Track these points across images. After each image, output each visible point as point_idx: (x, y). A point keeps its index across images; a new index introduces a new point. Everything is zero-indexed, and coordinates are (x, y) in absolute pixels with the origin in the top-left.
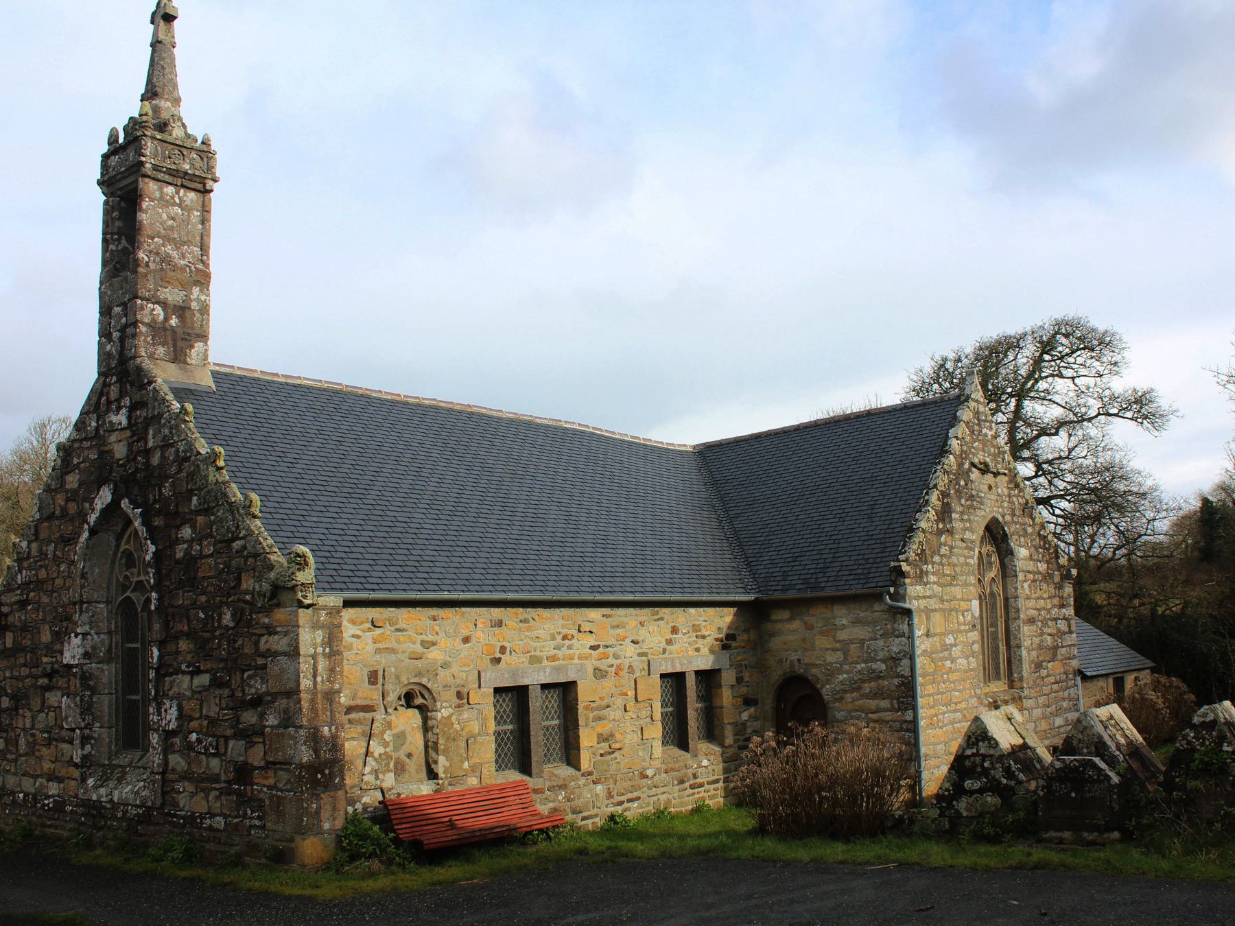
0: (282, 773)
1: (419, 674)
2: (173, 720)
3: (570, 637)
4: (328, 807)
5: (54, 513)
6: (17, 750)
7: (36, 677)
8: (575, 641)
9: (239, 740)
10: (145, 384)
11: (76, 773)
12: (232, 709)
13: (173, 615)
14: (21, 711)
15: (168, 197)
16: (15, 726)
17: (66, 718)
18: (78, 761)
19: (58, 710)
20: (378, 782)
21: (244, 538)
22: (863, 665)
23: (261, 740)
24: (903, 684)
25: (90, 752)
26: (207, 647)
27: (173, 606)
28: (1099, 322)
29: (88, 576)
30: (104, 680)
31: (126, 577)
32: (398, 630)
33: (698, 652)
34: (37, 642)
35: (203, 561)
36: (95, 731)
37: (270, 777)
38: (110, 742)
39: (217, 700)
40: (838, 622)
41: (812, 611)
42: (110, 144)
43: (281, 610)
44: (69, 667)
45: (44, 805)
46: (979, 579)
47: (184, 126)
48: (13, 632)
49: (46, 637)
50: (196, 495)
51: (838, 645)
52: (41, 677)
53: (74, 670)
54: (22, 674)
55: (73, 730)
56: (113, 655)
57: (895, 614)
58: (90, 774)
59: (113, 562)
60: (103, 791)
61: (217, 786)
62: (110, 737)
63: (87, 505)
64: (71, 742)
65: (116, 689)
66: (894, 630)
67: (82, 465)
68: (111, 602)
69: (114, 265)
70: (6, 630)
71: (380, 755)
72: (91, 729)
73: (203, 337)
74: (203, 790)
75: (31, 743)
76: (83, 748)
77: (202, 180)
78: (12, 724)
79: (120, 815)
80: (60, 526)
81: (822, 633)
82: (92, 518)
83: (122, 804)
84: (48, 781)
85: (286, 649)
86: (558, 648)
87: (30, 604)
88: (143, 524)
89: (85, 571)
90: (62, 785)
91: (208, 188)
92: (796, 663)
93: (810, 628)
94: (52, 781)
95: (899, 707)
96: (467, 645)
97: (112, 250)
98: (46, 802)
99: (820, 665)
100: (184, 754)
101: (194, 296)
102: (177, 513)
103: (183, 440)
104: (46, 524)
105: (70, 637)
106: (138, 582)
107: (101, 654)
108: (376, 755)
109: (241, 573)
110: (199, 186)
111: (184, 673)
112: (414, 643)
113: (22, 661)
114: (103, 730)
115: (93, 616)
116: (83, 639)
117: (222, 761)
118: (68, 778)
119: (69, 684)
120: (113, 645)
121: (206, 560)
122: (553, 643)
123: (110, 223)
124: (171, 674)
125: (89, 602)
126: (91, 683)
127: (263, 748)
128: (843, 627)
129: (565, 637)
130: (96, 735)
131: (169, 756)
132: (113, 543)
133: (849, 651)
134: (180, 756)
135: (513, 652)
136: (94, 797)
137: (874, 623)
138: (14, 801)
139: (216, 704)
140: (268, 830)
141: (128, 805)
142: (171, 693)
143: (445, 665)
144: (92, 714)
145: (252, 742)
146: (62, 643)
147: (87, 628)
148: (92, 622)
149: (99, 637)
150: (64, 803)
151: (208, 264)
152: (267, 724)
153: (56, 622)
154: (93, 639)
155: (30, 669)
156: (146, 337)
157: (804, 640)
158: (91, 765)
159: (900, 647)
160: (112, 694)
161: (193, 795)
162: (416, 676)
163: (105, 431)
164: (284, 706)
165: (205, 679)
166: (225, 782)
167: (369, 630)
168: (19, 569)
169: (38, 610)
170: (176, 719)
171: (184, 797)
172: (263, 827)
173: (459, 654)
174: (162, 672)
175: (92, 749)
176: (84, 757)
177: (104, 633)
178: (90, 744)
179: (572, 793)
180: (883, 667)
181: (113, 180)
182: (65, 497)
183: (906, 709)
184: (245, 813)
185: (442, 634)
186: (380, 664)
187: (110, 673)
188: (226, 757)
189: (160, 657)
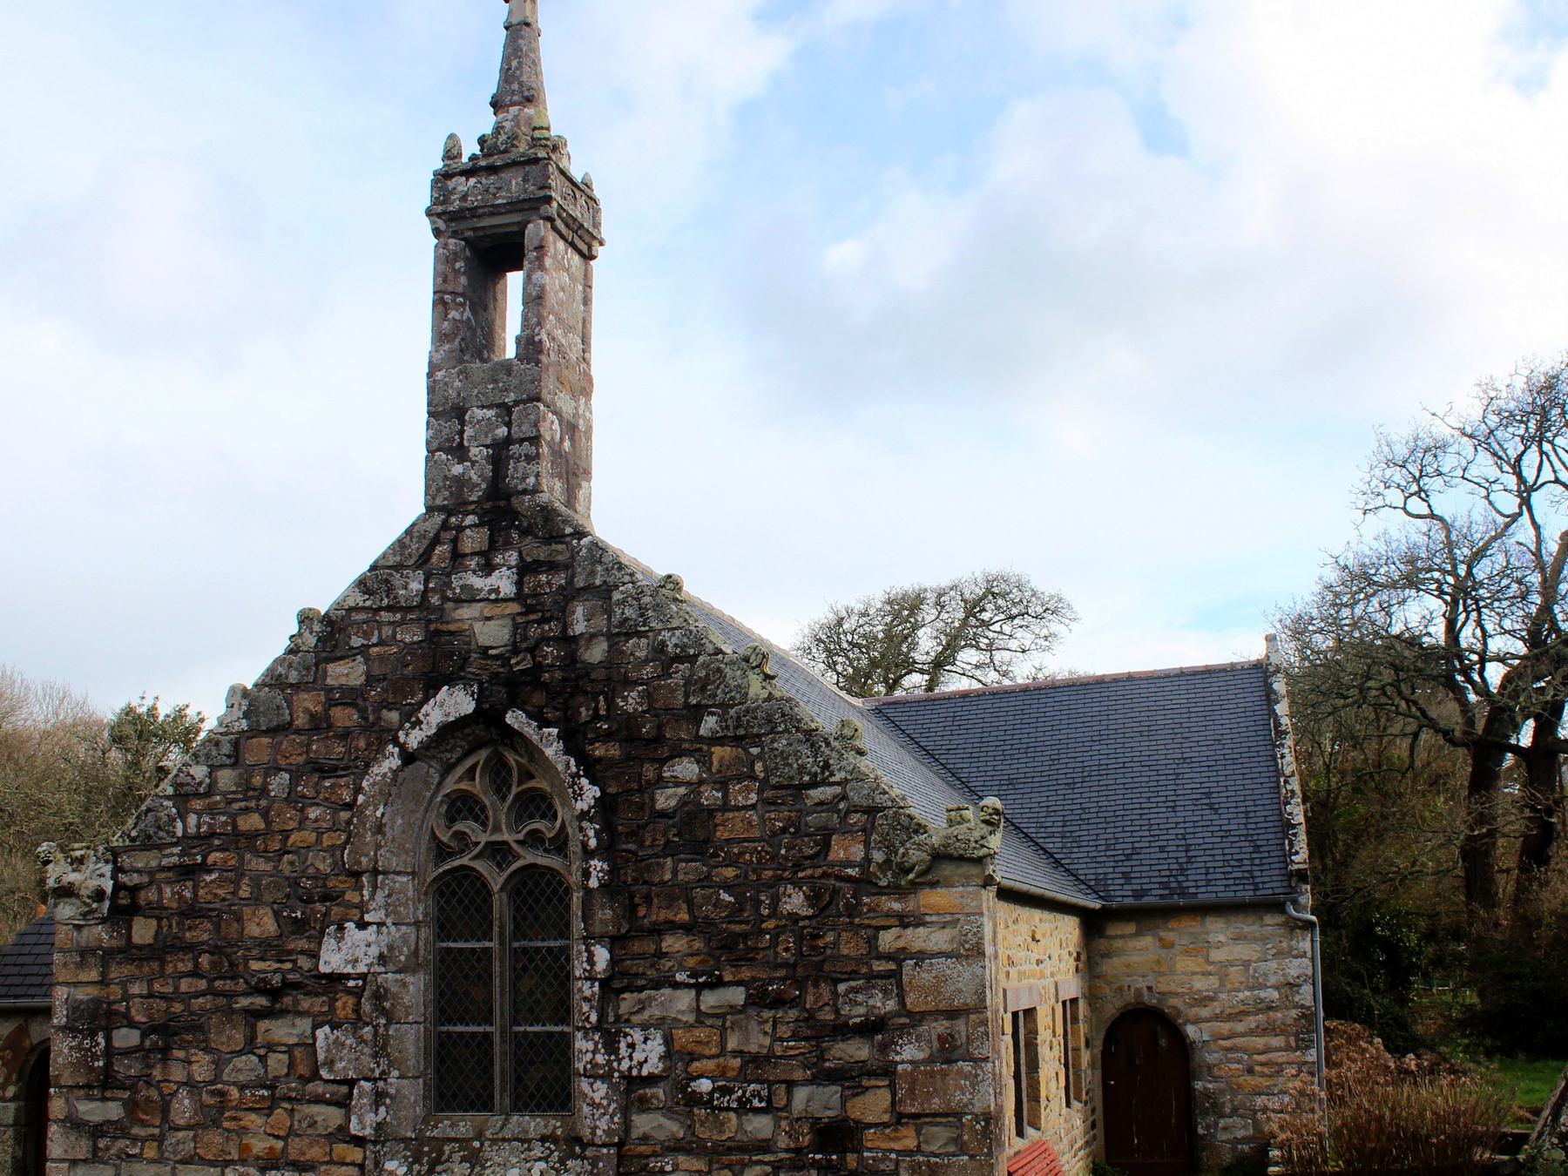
5: (291, 723)
7: (231, 995)
12: (806, 1039)
17: (330, 1063)
21: (843, 783)
22: (1247, 993)
23: (886, 1083)
24: (1304, 1016)
26: (741, 946)
27: (646, 882)
28: (1043, 582)
29: (387, 829)
36: (391, 1084)
39: (768, 1028)
40: (1212, 938)
41: (1172, 924)
43: (939, 890)
44: (336, 978)
51: (1210, 968)
52: (246, 994)
55: (351, 1083)
56: (421, 960)
57: (1292, 929)
66: (1291, 948)
67: (376, 649)
72: (385, 1080)
81: (1187, 952)
82: (414, 739)
87: (210, 872)
88: (568, 751)
92: (1145, 991)
93: (1166, 945)
95: (1297, 1045)
99: (1183, 994)
100: (676, 1112)
104: (265, 740)
105: (341, 928)
107: (402, 958)
109: (831, 835)
114: (405, 1082)
115: (389, 896)
125: (385, 873)
126: (387, 1005)
127: (889, 1097)
128: (1220, 945)
130: (392, 1091)
131: (634, 1117)
132: (437, 778)
133: (1227, 975)
137: (1264, 939)
145: (860, 1086)
147: (382, 914)
148: (388, 904)
149: (398, 930)
152: (898, 1058)
154: (389, 933)
157: (1158, 962)
158: (386, 1140)
159: (1300, 971)
169: (236, 883)
170: (661, 1058)
174: (616, 984)
177: (407, 924)
180: (1276, 995)
183: (1308, 1047)
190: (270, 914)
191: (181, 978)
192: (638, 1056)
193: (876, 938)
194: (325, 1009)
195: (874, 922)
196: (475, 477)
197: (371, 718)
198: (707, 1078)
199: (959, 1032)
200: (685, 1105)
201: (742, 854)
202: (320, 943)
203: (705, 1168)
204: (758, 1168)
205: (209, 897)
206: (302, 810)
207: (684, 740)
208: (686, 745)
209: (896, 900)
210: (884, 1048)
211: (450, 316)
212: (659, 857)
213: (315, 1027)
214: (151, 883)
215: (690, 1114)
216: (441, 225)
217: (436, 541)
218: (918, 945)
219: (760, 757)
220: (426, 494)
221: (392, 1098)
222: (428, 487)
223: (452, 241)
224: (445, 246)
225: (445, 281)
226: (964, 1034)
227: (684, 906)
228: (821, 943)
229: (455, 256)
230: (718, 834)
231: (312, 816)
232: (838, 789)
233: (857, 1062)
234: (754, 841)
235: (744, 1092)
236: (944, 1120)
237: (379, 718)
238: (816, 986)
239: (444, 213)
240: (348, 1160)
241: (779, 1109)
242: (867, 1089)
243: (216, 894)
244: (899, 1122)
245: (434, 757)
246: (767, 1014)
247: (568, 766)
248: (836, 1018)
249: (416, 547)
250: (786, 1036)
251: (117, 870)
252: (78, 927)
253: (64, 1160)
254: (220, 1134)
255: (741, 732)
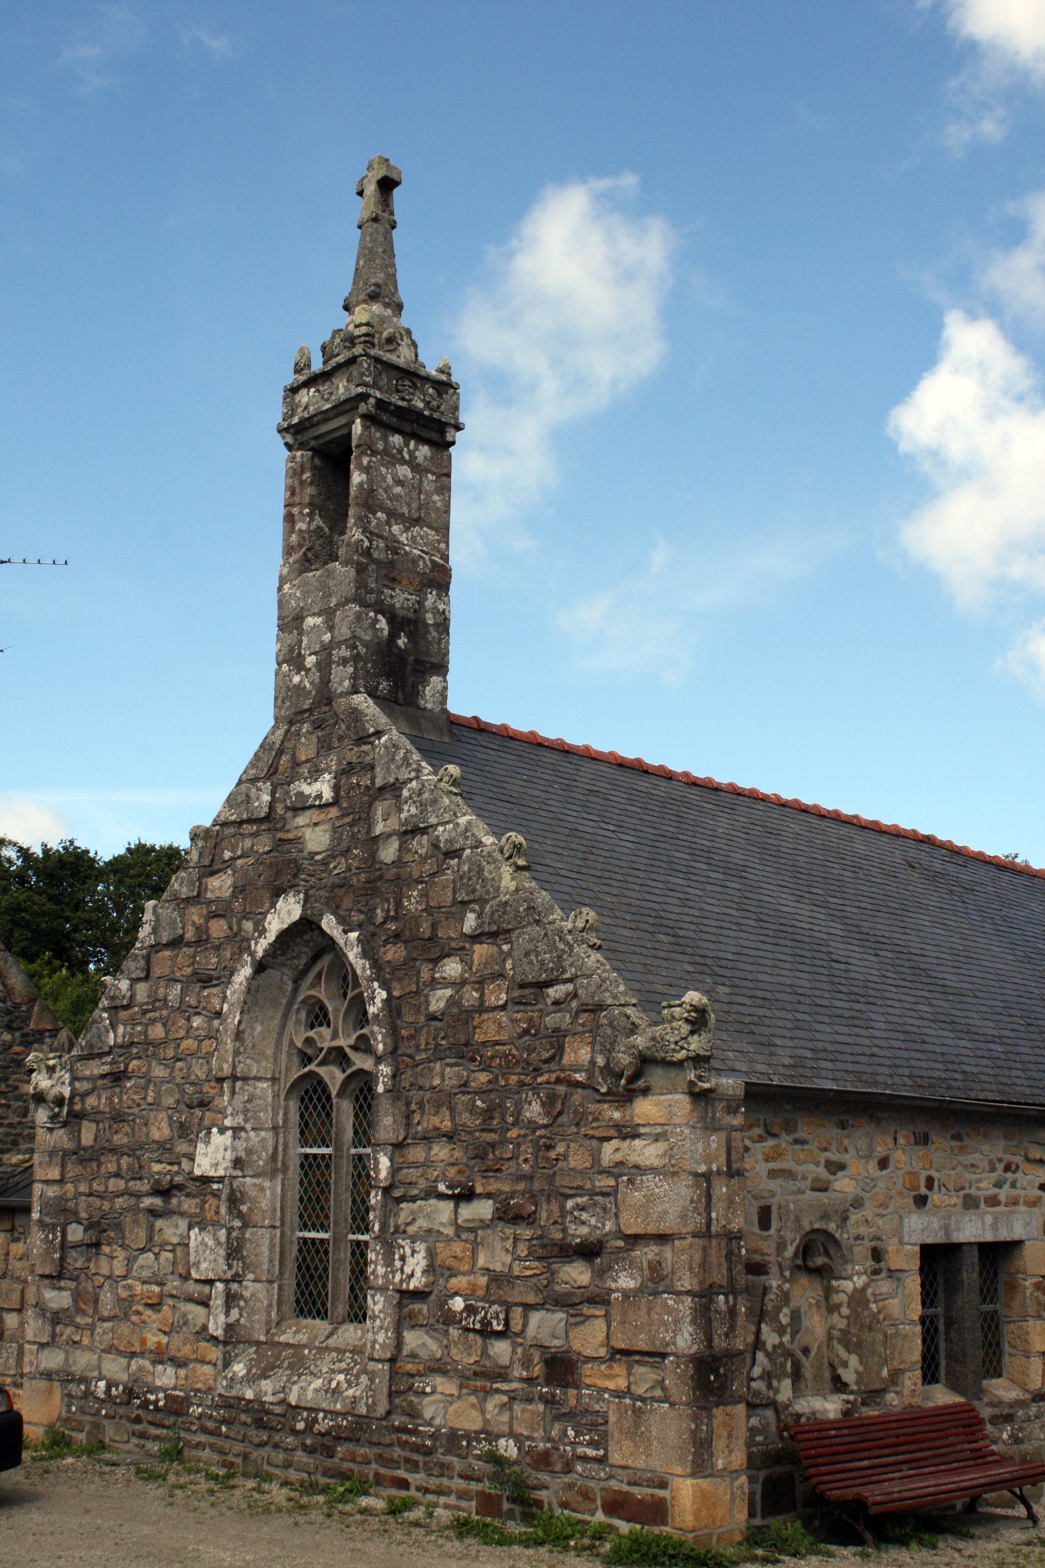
0: (643, 1369)
1: (825, 1217)
2: (418, 1274)
3: (1013, 1167)
4: (723, 1432)
5: (182, 937)
6: (96, 1310)
7: (138, 1196)
8: (1019, 1174)
9: (554, 1311)
10: (370, 736)
11: (215, 1353)
12: (539, 1259)
13: (421, 1105)
14: (106, 1249)
15: (395, 451)
16: (93, 1271)
17: (197, 1264)
18: (219, 1333)
19: (179, 1249)
20: (771, 1393)
23: (603, 1313)
25: (238, 1321)
26: (491, 1156)
27: (421, 1088)
29: (246, 1036)
30: (264, 1204)
31: (309, 1041)
32: (797, 1141)
33: (966, 1197)
34: (143, 1139)
35: (485, 1016)
37: (618, 1375)
38: (270, 1305)
39: (509, 1244)
42: (298, 370)
44: (206, 1180)
45: (147, 1402)
46: (369, 1110)
47: (414, 345)
48: (97, 1122)
49: (160, 1130)
50: (473, 911)
52: (148, 1194)
53: (215, 1186)
54: (111, 1189)
55: (210, 1282)
58: (236, 1356)
59: (285, 1017)
60: (267, 1385)
61: (505, 1387)
62: (270, 1296)
63: (248, 926)
64: (205, 1303)
65: (282, 1220)
67: (239, 862)
68: (279, 1079)
69: (305, 554)
70: (81, 1119)
71: (774, 1347)
72: (240, 1282)
73: (441, 668)
74: (475, 1391)
75: (124, 1300)
76: (227, 1314)
77: (441, 427)
78: (88, 1268)
79: (300, 1426)
80: (194, 957)
82: (261, 947)
83: (306, 1409)
84: (154, 1363)
85: (656, 1162)
86: (999, 1185)
87: (130, 1078)
88: (364, 954)
89: (241, 1028)
90: (182, 1372)
91: (449, 438)
94: (161, 1362)
96: (885, 1172)
97: (300, 531)
98: (152, 1397)
101: (429, 603)
102: (433, 938)
103: (448, 823)
104: (167, 953)
105: (209, 1133)
106: (331, 1050)
107: (261, 1163)
108: (769, 1348)
110: (435, 436)
111: (441, 1196)
112: (817, 1164)
113: (112, 1167)
115: (249, 1101)
116: (235, 1137)
117: (515, 1345)
118: (196, 1360)
119: (202, 1208)
120: (280, 1148)
121: (491, 1015)
122: (994, 1176)
123: (297, 490)
124: (413, 1199)
125: (245, 1079)
126: (244, 1208)
127: (605, 1329)
129: (1007, 1168)
130: (247, 1294)
131: (405, 1334)
132: (290, 986)
134: (427, 1333)
135: (943, 1188)
136: (249, 1394)
138: (88, 1394)
139: (507, 1251)
140: (612, 1466)
141: (317, 1410)
142: (411, 1229)
143: (857, 1203)
144: (243, 1258)
146: (193, 1143)
147: (240, 1119)
150: (186, 1402)
151: (448, 556)
152: (613, 1285)
153: (183, 1107)
154: (247, 1139)
155: (127, 1182)
156: (366, 663)
160: (274, 1227)
161: (450, 1399)
162: (822, 1218)
163: (287, 809)
164: (651, 1256)
165: (484, 1209)
166: (522, 1380)
167: (761, 1139)
168: (111, 1023)
169: (145, 1088)
170: (424, 1272)
171: (433, 1402)
172: (601, 1461)
173: (875, 1186)
174: (397, 1193)
175: (241, 1315)
176: (229, 1328)
177: (266, 1130)
178: (238, 1306)
179: (1020, 1429)
181: (307, 424)
182: (205, 912)
184: (564, 1433)
185: (852, 1151)
186: (773, 1196)
187: (274, 1194)
188: (524, 1338)
189: (394, 1170)
190: (166, 1119)
191: (110, 1178)
192: (408, 1270)
193: (599, 1151)
194: (198, 1211)
195: (596, 1133)
196: (308, 685)
197: (235, 928)
198: (461, 1296)
199: (666, 1259)
200: (443, 1324)
201: (493, 1057)
202: (196, 1146)
203: (455, 1392)
204: (497, 1396)
205: (130, 1103)
206: (188, 1019)
207: (452, 939)
208: (453, 944)
209: (617, 1109)
210: (600, 1273)
211: (297, 528)
212: (430, 1062)
213: (190, 1227)
214: (94, 1089)
215: (446, 1333)
216: (289, 439)
217: (280, 752)
218: (634, 1159)
219: (509, 954)
220: (275, 706)
221: (246, 1301)
222: (276, 698)
223: (299, 454)
224: (293, 459)
225: (293, 494)
226: (669, 1262)
227: (447, 1113)
228: (553, 1155)
229: (303, 469)
230: (476, 1036)
231: (195, 1025)
232: (570, 987)
233: (579, 1287)
234: (504, 1045)
235: (486, 1314)
236: (651, 1360)
237: (240, 929)
238: (548, 1201)
239: (290, 427)
240: (207, 1359)
241: (516, 1334)
242: (589, 1317)
243: (133, 1100)
244: (612, 1359)
245: (283, 964)
246: (509, 1231)
247: (364, 969)
248: (564, 1238)
249: (268, 759)
250: (523, 1255)
251: (74, 1079)
252: (51, 1130)
253: (35, 1343)
254: (129, 1327)
255: (494, 928)
